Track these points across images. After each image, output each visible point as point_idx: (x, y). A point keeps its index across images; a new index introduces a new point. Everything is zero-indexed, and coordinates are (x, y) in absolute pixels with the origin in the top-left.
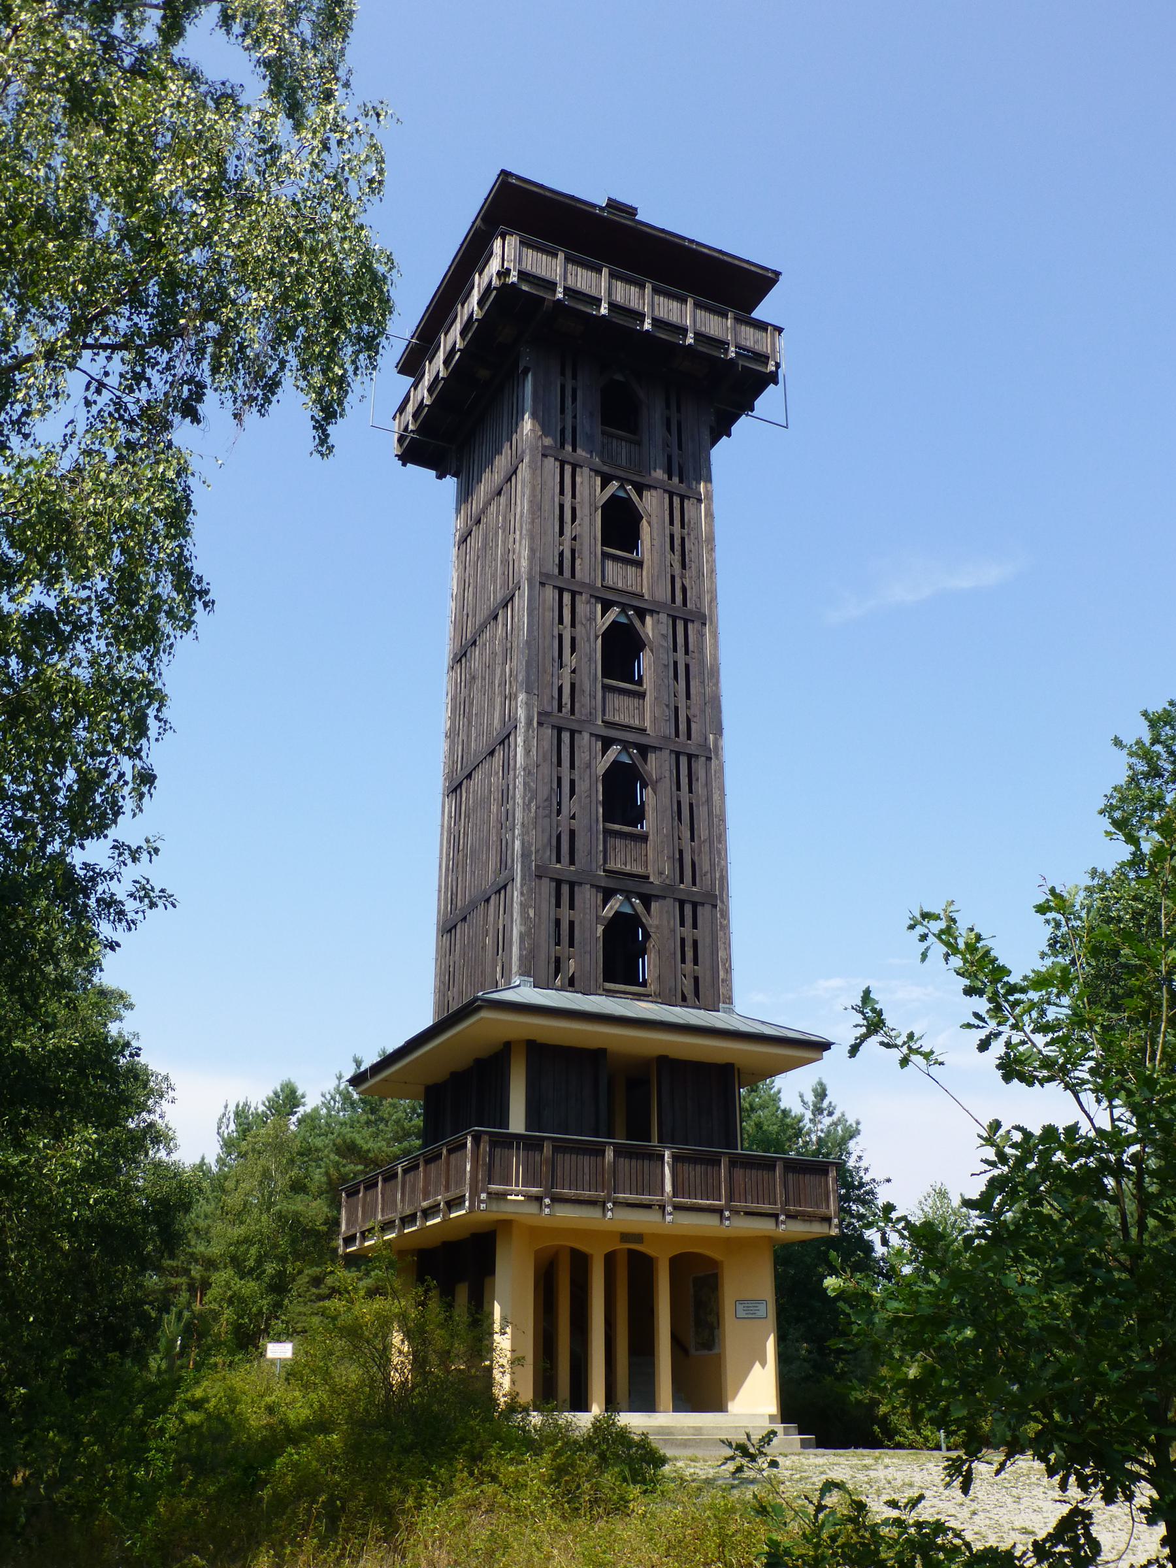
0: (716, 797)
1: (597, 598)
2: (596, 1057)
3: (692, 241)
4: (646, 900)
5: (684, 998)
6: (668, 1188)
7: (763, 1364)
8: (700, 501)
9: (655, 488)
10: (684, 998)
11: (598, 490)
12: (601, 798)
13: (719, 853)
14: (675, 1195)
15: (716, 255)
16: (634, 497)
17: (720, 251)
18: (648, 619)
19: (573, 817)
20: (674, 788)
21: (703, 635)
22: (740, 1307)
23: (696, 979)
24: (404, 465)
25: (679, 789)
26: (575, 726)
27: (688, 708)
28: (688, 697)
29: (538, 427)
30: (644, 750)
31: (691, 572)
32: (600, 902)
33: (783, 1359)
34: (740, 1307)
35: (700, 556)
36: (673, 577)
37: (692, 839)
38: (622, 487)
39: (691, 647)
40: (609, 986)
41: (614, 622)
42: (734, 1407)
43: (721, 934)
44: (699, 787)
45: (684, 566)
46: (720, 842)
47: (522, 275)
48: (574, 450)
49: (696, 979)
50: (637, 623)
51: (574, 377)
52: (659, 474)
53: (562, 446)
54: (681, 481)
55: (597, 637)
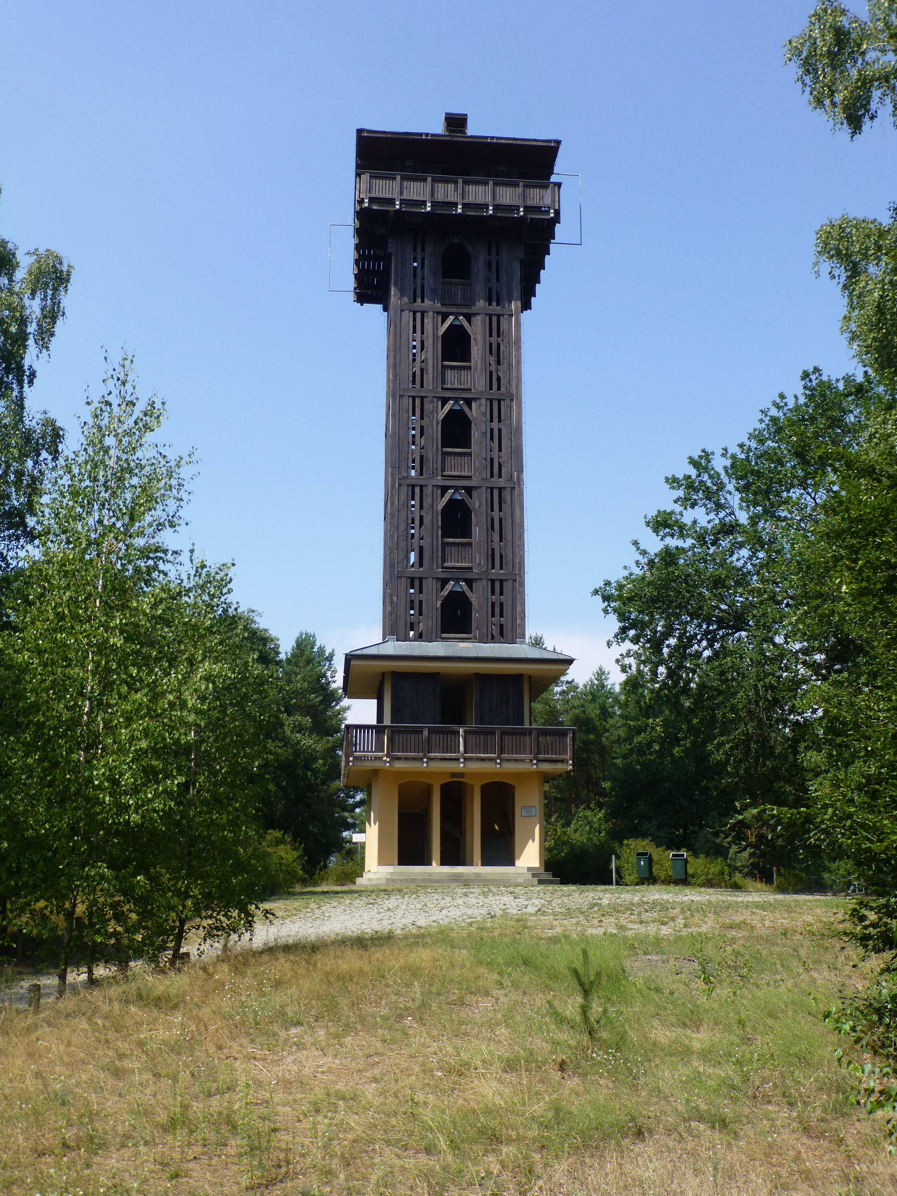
0: (517, 512)
1: (437, 397)
2: (434, 676)
3: (492, 138)
4: (470, 583)
5: (493, 637)
6: (462, 749)
7: (533, 841)
8: (511, 315)
9: (479, 314)
10: (493, 637)
11: (440, 324)
12: (440, 524)
13: (519, 546)
14: (466, 752)
15: (511, 142)
16: (465, 324)
17: (514, 139)
18: (474, 405)
19: (422, 539)
20: (489, 510)
21: (511, 408)
22: (523, 811)
23: (502, 626)
24: (362, 305)
25: (492, 510)
26: (423, 483)
27: (499, 457)
28: (500, 450)
29: (398, 293)
30: (469, 490)
31: (503, 367)
32: (439, 587)
33: (543, 839)
34: (523, 811)
35: (510, 354)
36: (491, 373)
37: (501, 540)
38: (456, 318)
39: (503, 418)
40: (444, 635)
41: (451, 410)
42: (517, 863)
43: (518, 597)
44: (506, 507)
45: (499, 363)
46: (520, 540)
47: (372, 200)
48: (423, 301)
49: (502, 626)
50: (466, 409)
51: (423, 250)
52: (481, 304)
53: (415, 301)
54: (498, 305)
55: (438, 423)
